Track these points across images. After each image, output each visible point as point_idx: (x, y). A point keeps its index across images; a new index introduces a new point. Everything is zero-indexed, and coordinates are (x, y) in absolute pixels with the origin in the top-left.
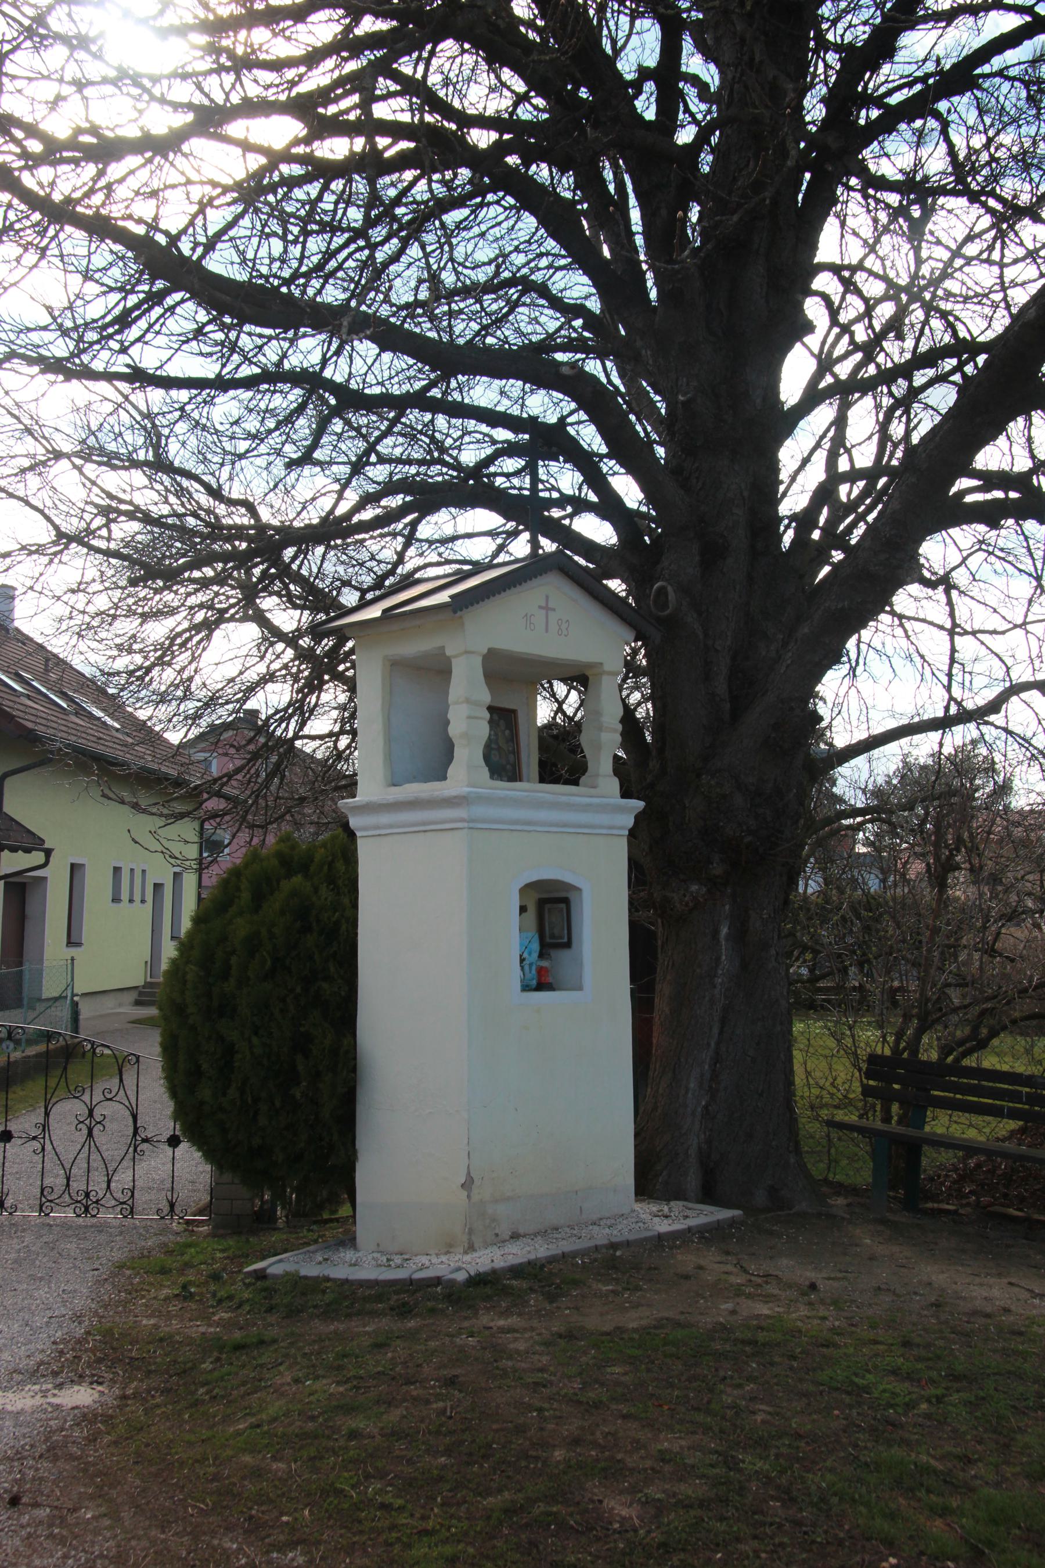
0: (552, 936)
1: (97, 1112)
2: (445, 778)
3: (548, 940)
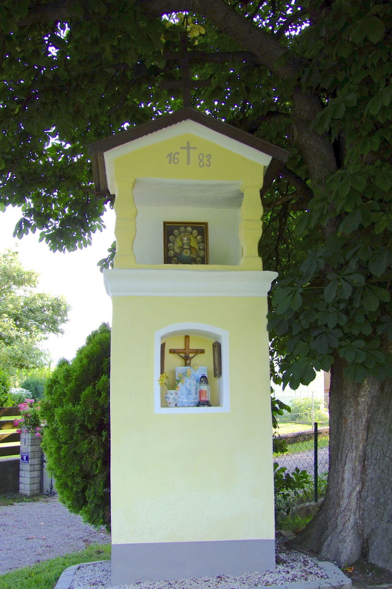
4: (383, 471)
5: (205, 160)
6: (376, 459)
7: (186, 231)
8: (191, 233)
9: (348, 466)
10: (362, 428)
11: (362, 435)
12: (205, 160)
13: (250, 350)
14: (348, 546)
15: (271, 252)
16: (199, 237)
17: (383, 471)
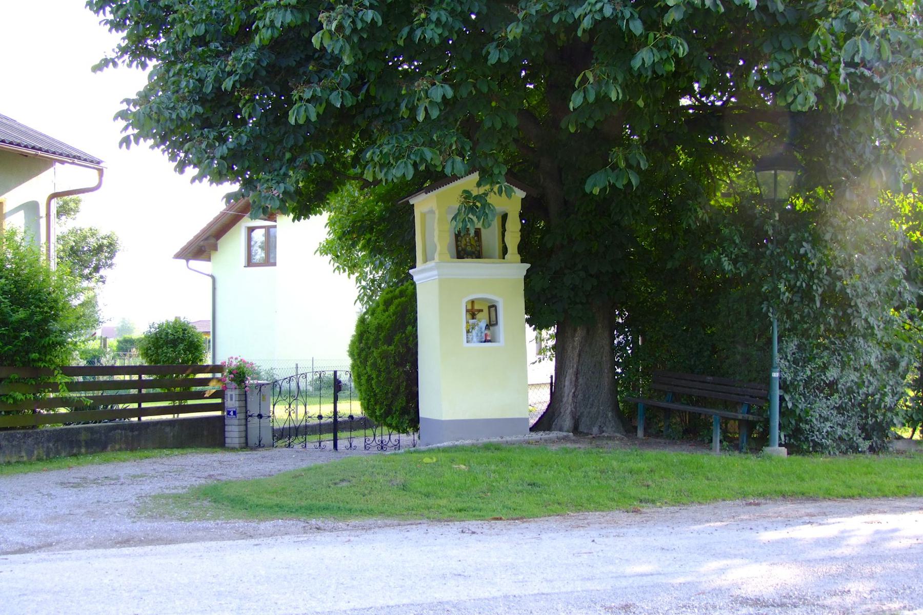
11: (576, 359)
13: (512, 308)
15: (525, 251)
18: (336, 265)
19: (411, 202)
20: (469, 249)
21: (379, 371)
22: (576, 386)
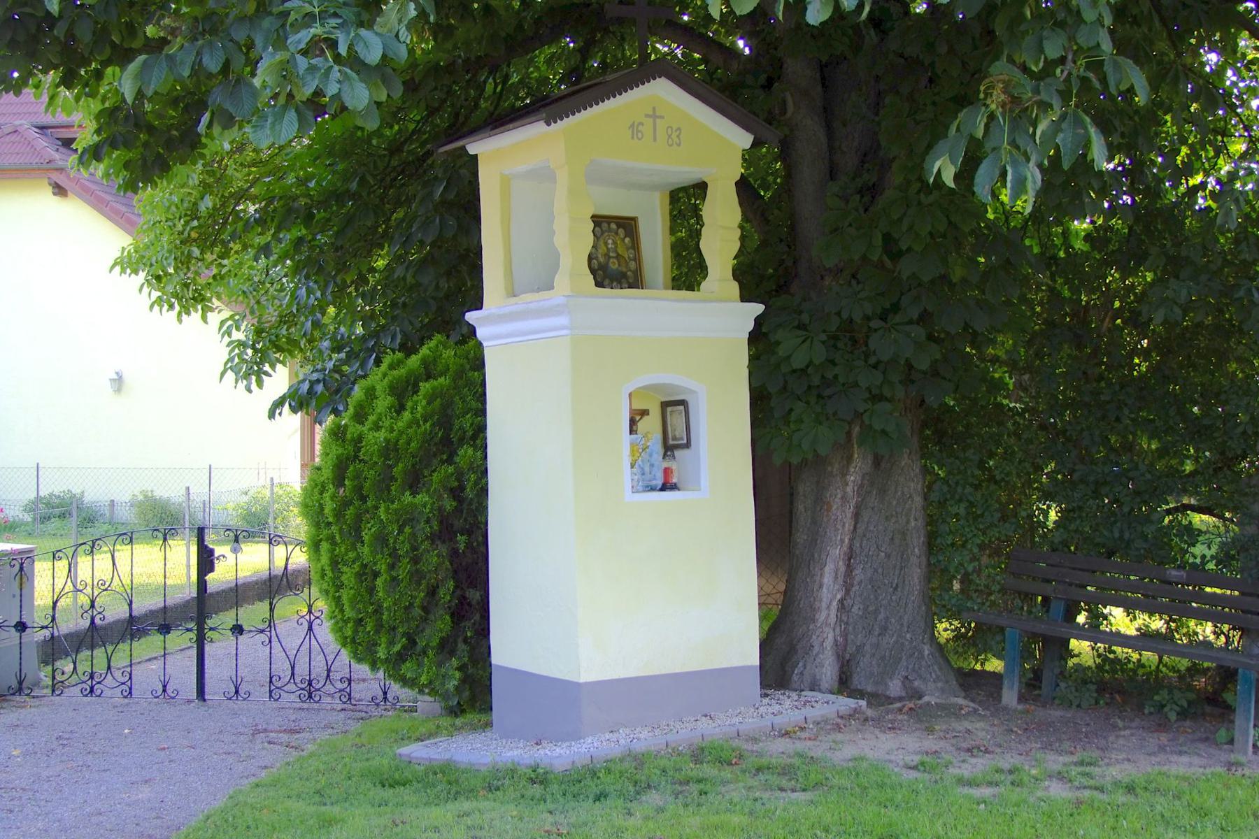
0: (674, 439)
1: (98, 602)
2: (552, 288)
3: (671, 442)
4: (876, 571)
5: (674, 136)
6: (867, 556)
7: (610, 230)
8: (617, 233)
9: (829, 569)
10: (849, 515)
11: (849, 525)
12: (674, 136)
14: (828, 670)
16: (627, 240)
17: (876, 571)
18: (156, 294)
19: (472, 149)
20: (614, 265)
21: (394, 554)
22: (848, 588)
